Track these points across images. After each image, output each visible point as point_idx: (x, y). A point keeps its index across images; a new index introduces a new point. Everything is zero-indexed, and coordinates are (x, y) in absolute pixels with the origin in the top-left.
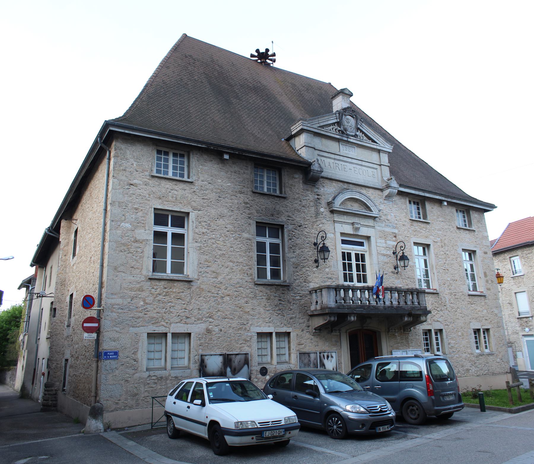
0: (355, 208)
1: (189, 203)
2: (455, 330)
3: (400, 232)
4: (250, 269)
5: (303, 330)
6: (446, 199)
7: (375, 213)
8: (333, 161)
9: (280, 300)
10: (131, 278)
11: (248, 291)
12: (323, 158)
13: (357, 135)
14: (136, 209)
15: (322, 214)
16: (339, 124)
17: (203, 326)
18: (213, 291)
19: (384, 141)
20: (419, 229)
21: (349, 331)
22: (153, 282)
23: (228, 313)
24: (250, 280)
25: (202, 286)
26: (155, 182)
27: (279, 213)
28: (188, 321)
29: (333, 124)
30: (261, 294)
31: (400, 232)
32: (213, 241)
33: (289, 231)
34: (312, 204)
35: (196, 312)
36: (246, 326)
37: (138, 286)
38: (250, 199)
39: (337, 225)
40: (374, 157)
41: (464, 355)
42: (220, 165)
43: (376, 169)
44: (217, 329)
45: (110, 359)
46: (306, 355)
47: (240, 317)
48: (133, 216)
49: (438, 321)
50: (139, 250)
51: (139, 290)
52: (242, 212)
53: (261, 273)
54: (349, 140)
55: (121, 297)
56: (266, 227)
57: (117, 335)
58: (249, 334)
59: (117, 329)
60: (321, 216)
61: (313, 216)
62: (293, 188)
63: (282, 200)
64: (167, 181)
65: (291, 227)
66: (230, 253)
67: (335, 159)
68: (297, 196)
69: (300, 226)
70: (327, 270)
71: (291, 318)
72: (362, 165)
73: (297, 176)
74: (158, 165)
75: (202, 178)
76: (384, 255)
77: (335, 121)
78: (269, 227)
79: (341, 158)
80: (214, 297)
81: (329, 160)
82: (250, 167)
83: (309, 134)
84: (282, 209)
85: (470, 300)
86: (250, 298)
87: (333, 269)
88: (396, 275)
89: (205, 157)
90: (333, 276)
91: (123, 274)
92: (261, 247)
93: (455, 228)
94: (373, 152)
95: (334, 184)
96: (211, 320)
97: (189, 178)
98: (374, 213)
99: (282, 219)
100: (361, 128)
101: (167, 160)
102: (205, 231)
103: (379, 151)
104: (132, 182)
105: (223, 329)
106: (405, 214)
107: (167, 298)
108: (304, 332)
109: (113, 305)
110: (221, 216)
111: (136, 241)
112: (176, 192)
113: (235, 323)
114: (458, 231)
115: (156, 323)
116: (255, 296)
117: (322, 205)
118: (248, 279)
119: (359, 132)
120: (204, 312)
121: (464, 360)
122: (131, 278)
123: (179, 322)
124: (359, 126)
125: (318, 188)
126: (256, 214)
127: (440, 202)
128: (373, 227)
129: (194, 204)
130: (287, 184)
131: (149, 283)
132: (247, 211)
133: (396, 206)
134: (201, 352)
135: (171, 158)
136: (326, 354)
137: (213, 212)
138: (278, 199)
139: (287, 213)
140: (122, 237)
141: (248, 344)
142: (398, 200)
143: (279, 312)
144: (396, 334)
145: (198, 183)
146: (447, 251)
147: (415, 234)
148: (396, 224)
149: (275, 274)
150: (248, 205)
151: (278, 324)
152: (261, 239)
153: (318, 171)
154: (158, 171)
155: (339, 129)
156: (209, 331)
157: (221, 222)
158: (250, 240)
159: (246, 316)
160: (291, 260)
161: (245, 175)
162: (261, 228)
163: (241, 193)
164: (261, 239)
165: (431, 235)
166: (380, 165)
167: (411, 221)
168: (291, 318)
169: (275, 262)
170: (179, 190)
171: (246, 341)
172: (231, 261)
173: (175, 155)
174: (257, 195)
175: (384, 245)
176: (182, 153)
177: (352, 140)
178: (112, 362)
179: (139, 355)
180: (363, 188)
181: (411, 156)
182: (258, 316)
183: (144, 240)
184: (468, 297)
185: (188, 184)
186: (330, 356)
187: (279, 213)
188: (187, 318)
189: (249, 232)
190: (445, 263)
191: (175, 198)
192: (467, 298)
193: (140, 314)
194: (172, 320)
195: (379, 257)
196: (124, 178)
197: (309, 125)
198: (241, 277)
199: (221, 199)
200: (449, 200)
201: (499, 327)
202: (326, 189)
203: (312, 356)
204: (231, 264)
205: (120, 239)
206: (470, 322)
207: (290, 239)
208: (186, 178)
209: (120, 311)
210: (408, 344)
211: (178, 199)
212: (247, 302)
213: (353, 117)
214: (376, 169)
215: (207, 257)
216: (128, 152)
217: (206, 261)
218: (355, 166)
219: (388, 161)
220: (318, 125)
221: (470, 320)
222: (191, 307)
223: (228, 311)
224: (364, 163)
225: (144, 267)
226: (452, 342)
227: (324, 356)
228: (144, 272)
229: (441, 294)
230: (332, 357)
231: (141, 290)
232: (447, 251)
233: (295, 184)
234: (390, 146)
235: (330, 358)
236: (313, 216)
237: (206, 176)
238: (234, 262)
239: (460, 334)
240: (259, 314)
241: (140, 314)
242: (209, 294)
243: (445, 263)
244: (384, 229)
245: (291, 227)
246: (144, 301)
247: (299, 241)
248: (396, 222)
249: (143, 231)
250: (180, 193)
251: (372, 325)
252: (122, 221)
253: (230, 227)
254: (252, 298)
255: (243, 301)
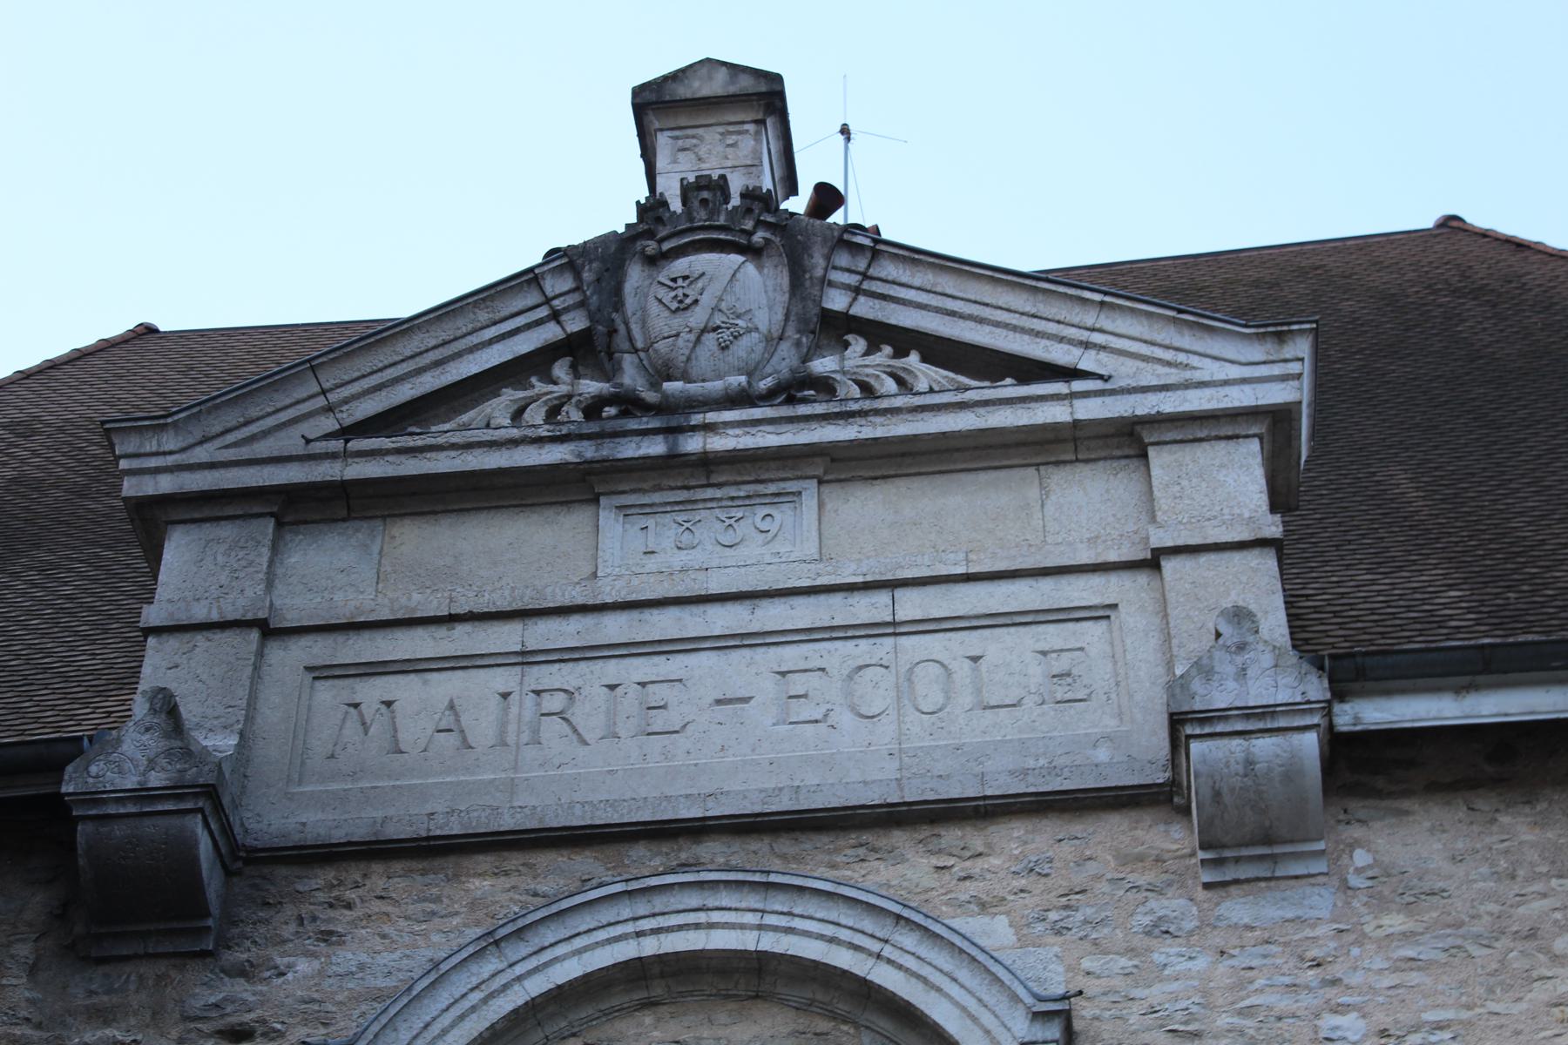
12: (370, 692)
16: (584, 350)
29: (536, 364)
40: (1084, 510)
43: (1103, 613)
54: (693, 444)
72: (893, 628)
79: (614, 628)
81: (445, 685)
83: (227, 531)
94: (1058, 479)
100: (865, 308)
103: (1128, 441)
114: (1209, 894)
124: (837, 301)
125: (244, 972)
133: (1395, 922)
166: (1152, 563)
181: (1392, 242)
197: (201, 454)
202: (346, 958)
213: (752, 252)
214: (1103, 613)
218: (791, 656)
220: (329, 424)
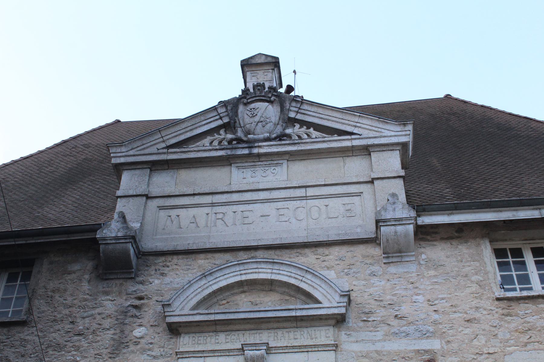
0: (270, 304)
15: (137, 343)
16: (228, 127)
29: (216, 130)
43: (359, 194)
54: (255, 151)
61: (105, 351)
67: (213, 205)
68: (67, 312)
72: (306, 198)
73: (76, 267)
83: (137, 172)
98: (326, 304)
100: (299, 117)
101: (522, 265)
103: (366, 151)
106: (474, 288)
117: (144, 321)
124: (292, 115)
125: (142, 283)
130: (41, 291)
133: (432, 273)
148: (435, 323)
166: (372, 182)
180: (307, 251)
197: (131, 153)
199: (418, 313)
202: (167, 279)
214: (359, 194)
218: (280, 205)
219: (400, 166)
220: (164, 145)
236: (105, 351)
244: (378, 346)
248: (436, 316)
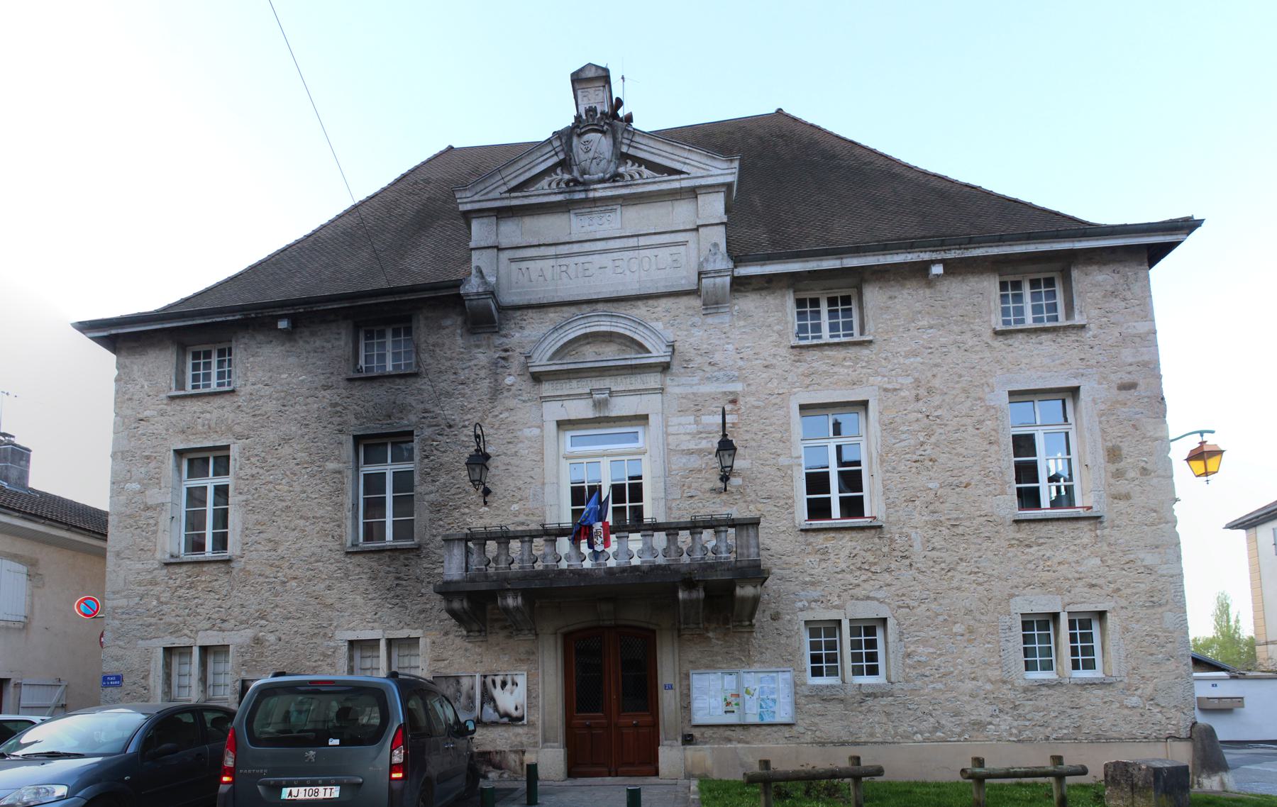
1: (230, 429)
2: (941, 618)
3: (753, 388)
4: (339, 526)
5: (446, 634)
6: (934, 256)
7: (658, 353)
8: (552, 262)
9: (398, 578)
10: (139, 566)
11: (333, 568)
12: (524, 265)
13: (622, 176)
14: (147, 457)
15: (509, 390)
16: (565, 164)
17: (249, 633)
18: (267, 573)
19: (704, 160)
20: (825, 368)
21: (565, 630)
22: (171, 569)
23: (292, 609)
24: (338, 547)
25: (248, 567)
26: (176, 405)
27: (403, 409)
28: (225, 625)
30: (358, 570)
31: (753, 388)
32: (270, 486)
33: (424, 440)
34: (483, 373)
35: (237, 610)
36: (327, 631)
37: (149, 577)
38: (345, 393)
39: (547, 406)
40: (682, 213)
41: (969, 685)
42: (288, 345)
43: (684, 243)
44: (272, 638)
45: (111, 686)
46: (452, 680)
47: (315, 615)
48: (143, 470)
49: (868, 598)
50: (152, 521)
51: (151, 584)
52: (325, 424)
53: (373, 532)
54: (591, 195)
55: (125, 597)
56: (386, 444)
57: (121, 652)
58: (332, 644)
59: (121, 643)
60: (506, 394)
62: (437, 350)
63: (411, 381)
64: (194, 400)
65: (428, 432)
66: (300, 503)
67: (557, 256)
68: (448, 364)
69: (450, 426)
70: (515, 507)
71: (423, 611)
72: (637, 248)
73: (448, 322)
74: (1005, 312)
75: (252, 380)
76: (690, 452)
77: (555, 160)
78: (393, 444)
79: (576, 248)
80: (269, 583)
81: (540, 264)
82: (343, 332)
83: (485, 220)
84: (410, 400)
85: (1018, 536)
86: (337, 578)
87: (530, 505)
88: (724, 496)
89: (260, 337)
90: (531, 517)
91: (128, 562)
92: (374, 483)
93: (989, 332)
95: (552, 315)
96: (263, 622)
97: (862, 333)
98: (655, 354)
99: (409, 421)
100: (632, 152)
102: (254, 471)
104: (140, 416)
105: (283, 637)
106: (775, 337)
107: (193, 592)
108: (451, 636)
109: (114, 608)
110: (286, 440)
111: (148, 508)
112: (208, 416)
113: (306, 625)
114: (998, 343)
115: (176, 631)
116: (347, 575)
117: (512, 371)
118: (334, 545)
119: (630, 163)
120: (252, 611)
121: (967, 698)
122: (139, 566)
123: (210, 629)
124: (624, 149)
125: (505, 336)
126: (354, 421)
127: (921, 270)
128: (662, 390)
129: (237, 429)
130: (423, 346)
131: (165, 571)
132: (337, 420)
134: (244, 675)
135: (389, 340)
136: (498, 680)
137: (271, 436)
138: (403, 381)
139: (422, 406)
140: (127, 505)
141: (329, 661)
142: (749, 303)
143: (394, 601)
144: (711, 634)
145: (244, 391)
146: (939, 407)
147: (807, 381)
148: (740, 369)
149: (403, 529)
150: (339, 409)
151: (393, 623)
152: (196, 483)
153: (478, 294)
154: (1006, 322)
155: (567, 177)
156: (258, 641)
157: (286, 450)
158: (340, 472)
159: (327, 613)
160: (427, 497)
161: (334, 353)
162: (370, 445)
163: (326, 388)
164: (196, 483)
165: (877, 374)
167: (795, 352)
168: (423, 611)
169: (404, 504)
170: (213, 411)
171: (325, 655)
172: (301, 517)
173: (1035, 284)
174: (357, 383)
175: (693, 428)
176: (844, 293)
177: (601, 192)
178: (115, 690)
179: (151, 681)
182: (350, 611)
183: (158, 505)
184: (1015, 527)
185: (227, 397)
186: (510, 683)
187: (403, 409)
188: (224, 621)
189: (338, 459)
190: (922, 444)
191: (206, 423)
192: (1012, 532)
193: (153, 620)
194: (199, 626)
195: (674, 458)
196: (129, 412)
197: (476, 198)
198: (321, 542)
200: (953, 254)
201: (1154, 605)
202: (526, 332)
203: (465, 683)
204: (302, 522)
205: (123, 509)
206: (1012, 596)
207: (427, 457)
208: (1062, 321)
209: (124, 616)
210: (749, 656)
211: (213, 425)
212: (329, 588)
214: (684, 243)
215: (260, 517)
216: (135, 367)
217: (258, 523)
218: (616, 255)
220: (505, 188)
221: (1016, 591)
222: (229, 604)
223: (292, 605)
224: (643, 241)
225: (158, 547)
226: (921, 649)
227: (494, 682)
228: (158, 555)
229: (885, 530)
230: (515, 684)
231: (153, 583)
232: (939, 407)
233: (447, 343)
234: (725, 165)
235: (509, 686)
237: (260, 374)
238: (307, 519)
239: (958, 628)
240: (354, 606)
241: (153, 620)
242: (261, 579)
243: (922, 444)
244: (695, 389)
245: (428, 432)
246: (158, 599)
247: (445, 458)
248: (741, 363)
249: (157, 490)
250: (216, 414)
251: (636, 616)
252: (127, 481)
253: (302, 456)
254: (340, 580)
255: (323, 586)
